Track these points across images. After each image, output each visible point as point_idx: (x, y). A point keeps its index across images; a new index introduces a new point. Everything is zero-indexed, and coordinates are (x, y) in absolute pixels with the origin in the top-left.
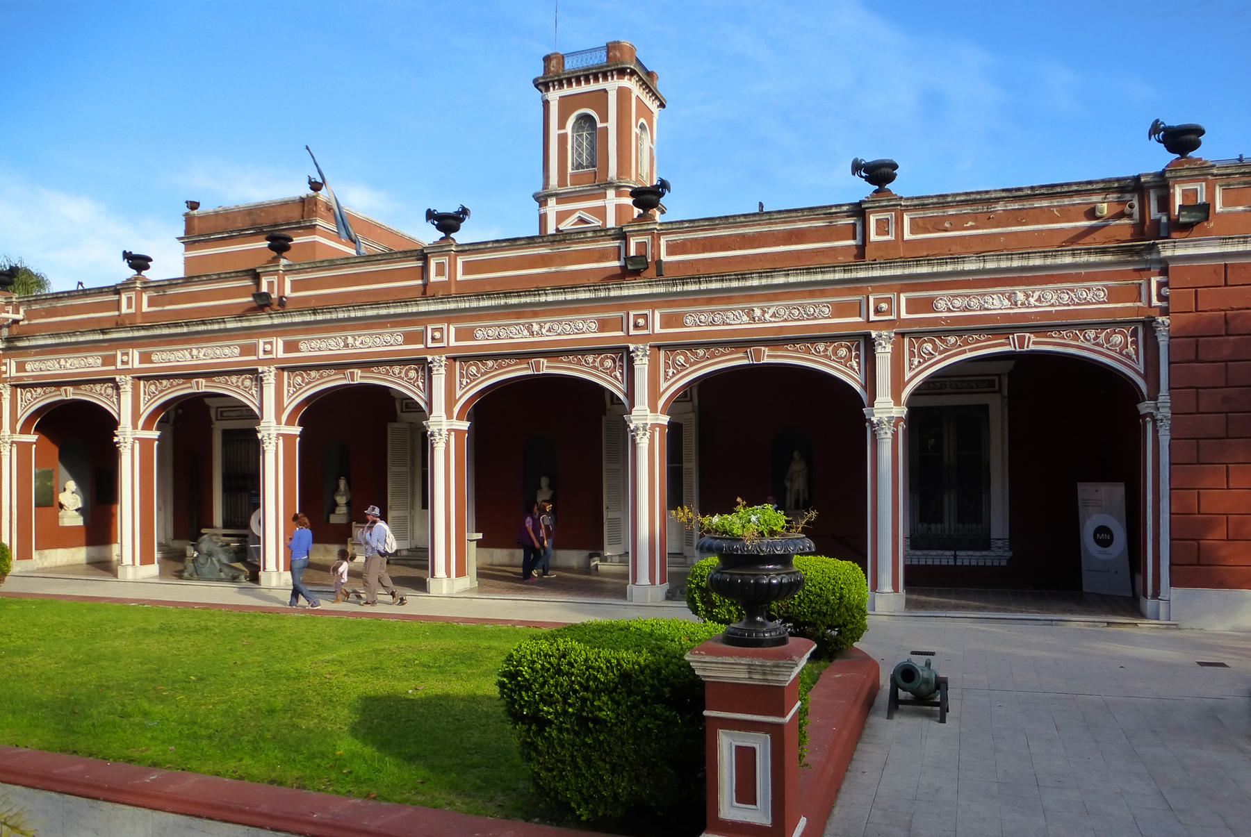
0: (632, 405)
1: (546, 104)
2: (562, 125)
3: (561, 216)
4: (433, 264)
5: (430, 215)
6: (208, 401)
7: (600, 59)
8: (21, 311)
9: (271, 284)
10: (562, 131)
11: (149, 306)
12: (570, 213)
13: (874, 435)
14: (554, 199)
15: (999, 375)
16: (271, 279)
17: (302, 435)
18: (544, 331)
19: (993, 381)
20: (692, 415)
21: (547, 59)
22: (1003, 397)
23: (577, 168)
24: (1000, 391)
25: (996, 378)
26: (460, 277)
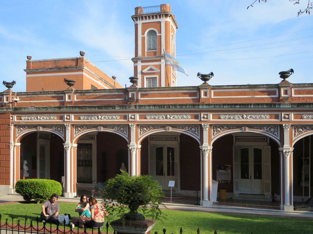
0: (130, 141)
1: (136, 26)
2: (143, 34)
3: (143, 68)
4: (202, 92)
5: (4, 83)
6: (232, 134)
7: (158, 10)
8: (18, 97)
9: (133, 95)
10: (143, 36)
11: (77, 99)
12: (147, 66)
13: (283, 155)
14: (140, 60)
15: (177, 136)
16: (133, 93)
17: (21, 146)
18: (248, 118)
19: (264, 139)
20: (178, 145)
21: (137, 9)
22: (268, 143)
23: (149, 50)
24: (267, 141)
25: (93, 136)
26: (212, 97)
